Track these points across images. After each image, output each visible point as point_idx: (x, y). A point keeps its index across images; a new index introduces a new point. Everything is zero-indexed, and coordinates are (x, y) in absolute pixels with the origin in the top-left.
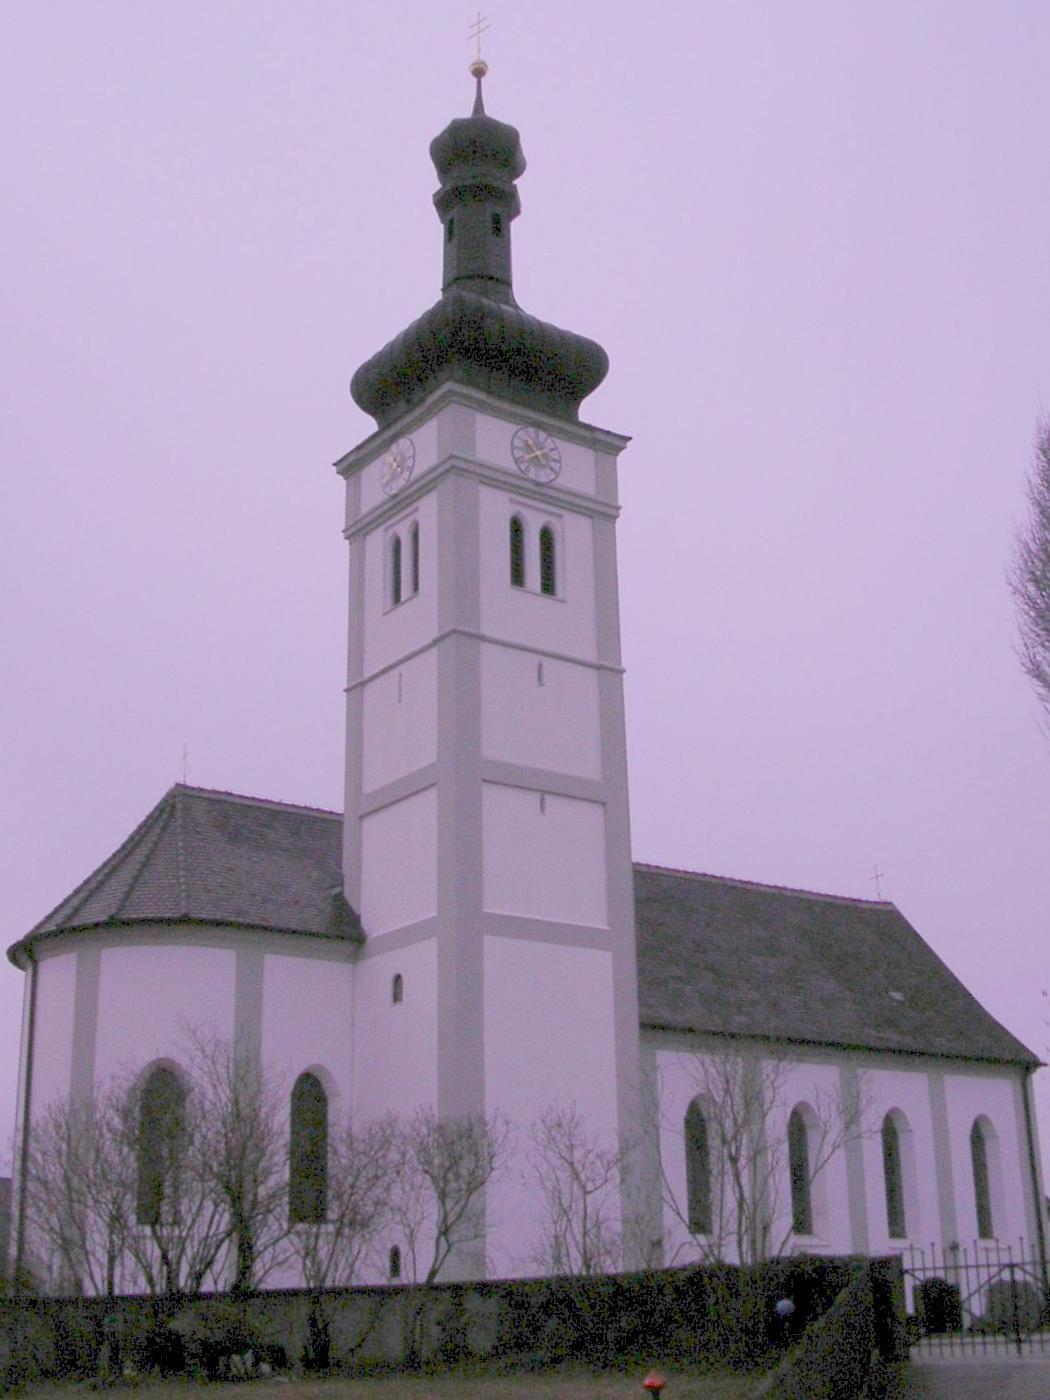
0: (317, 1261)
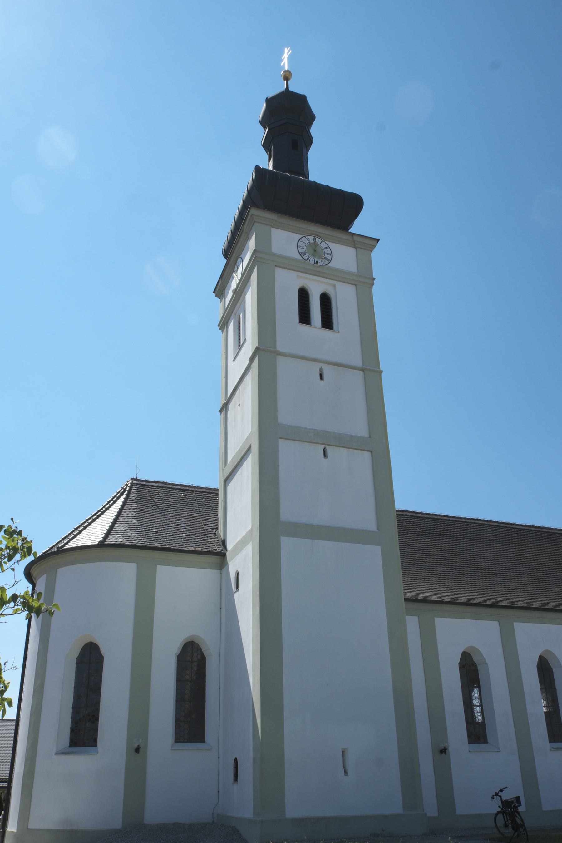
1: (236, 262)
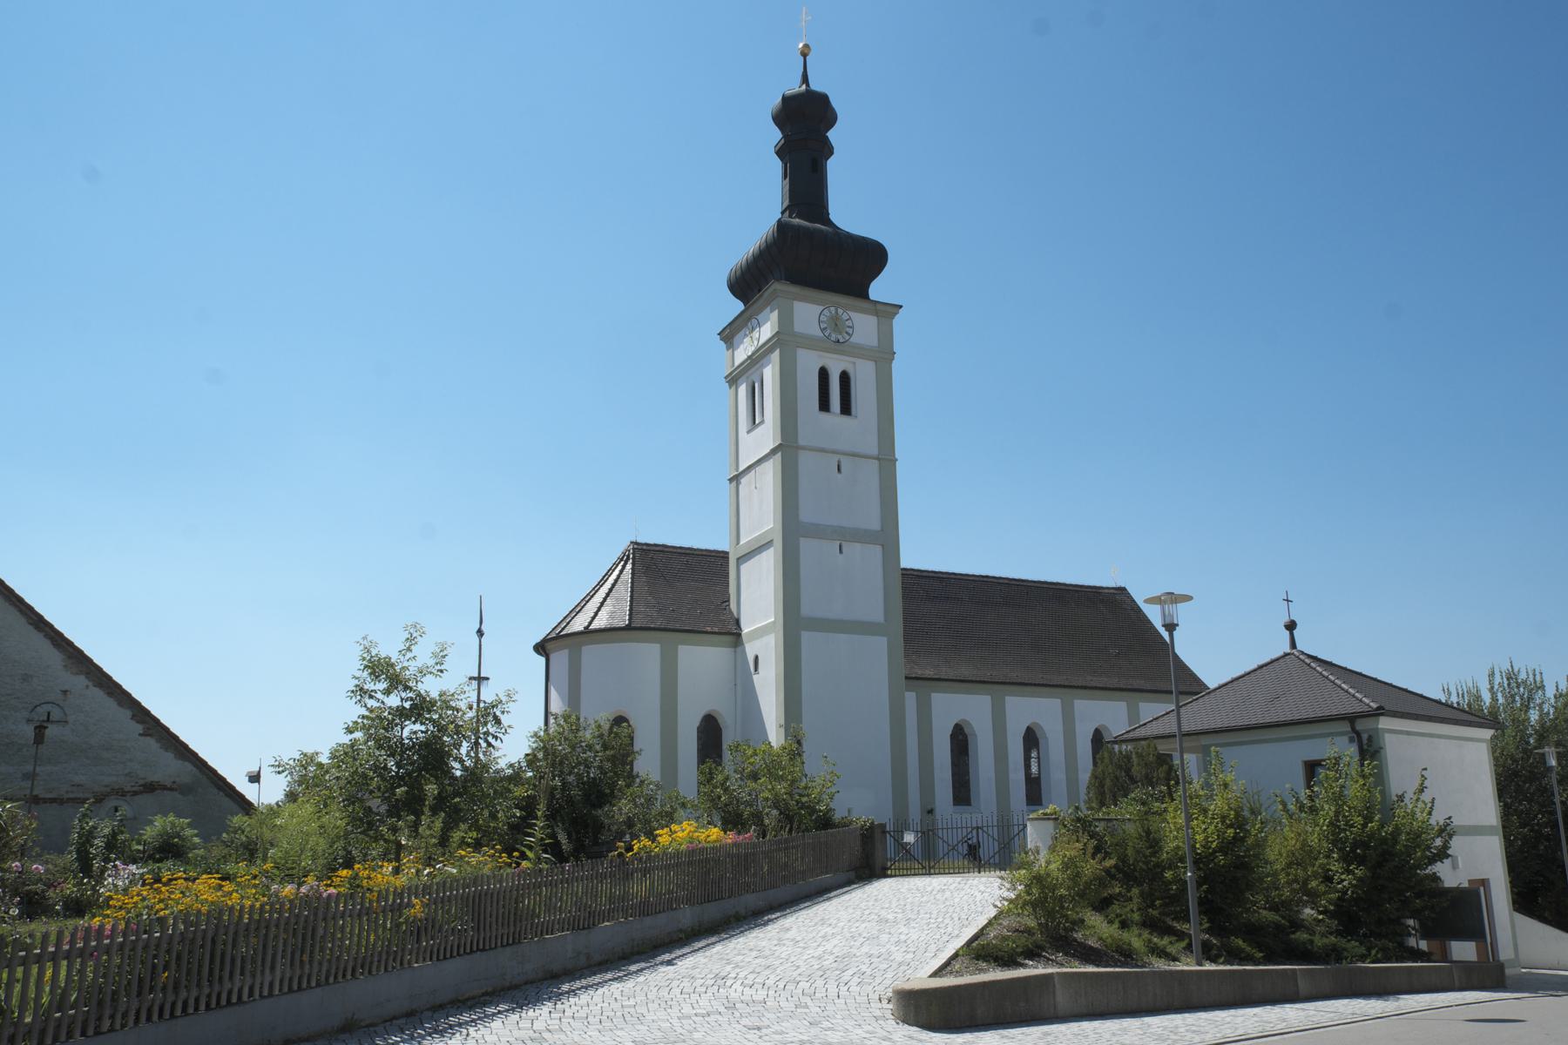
1: (749, 319)
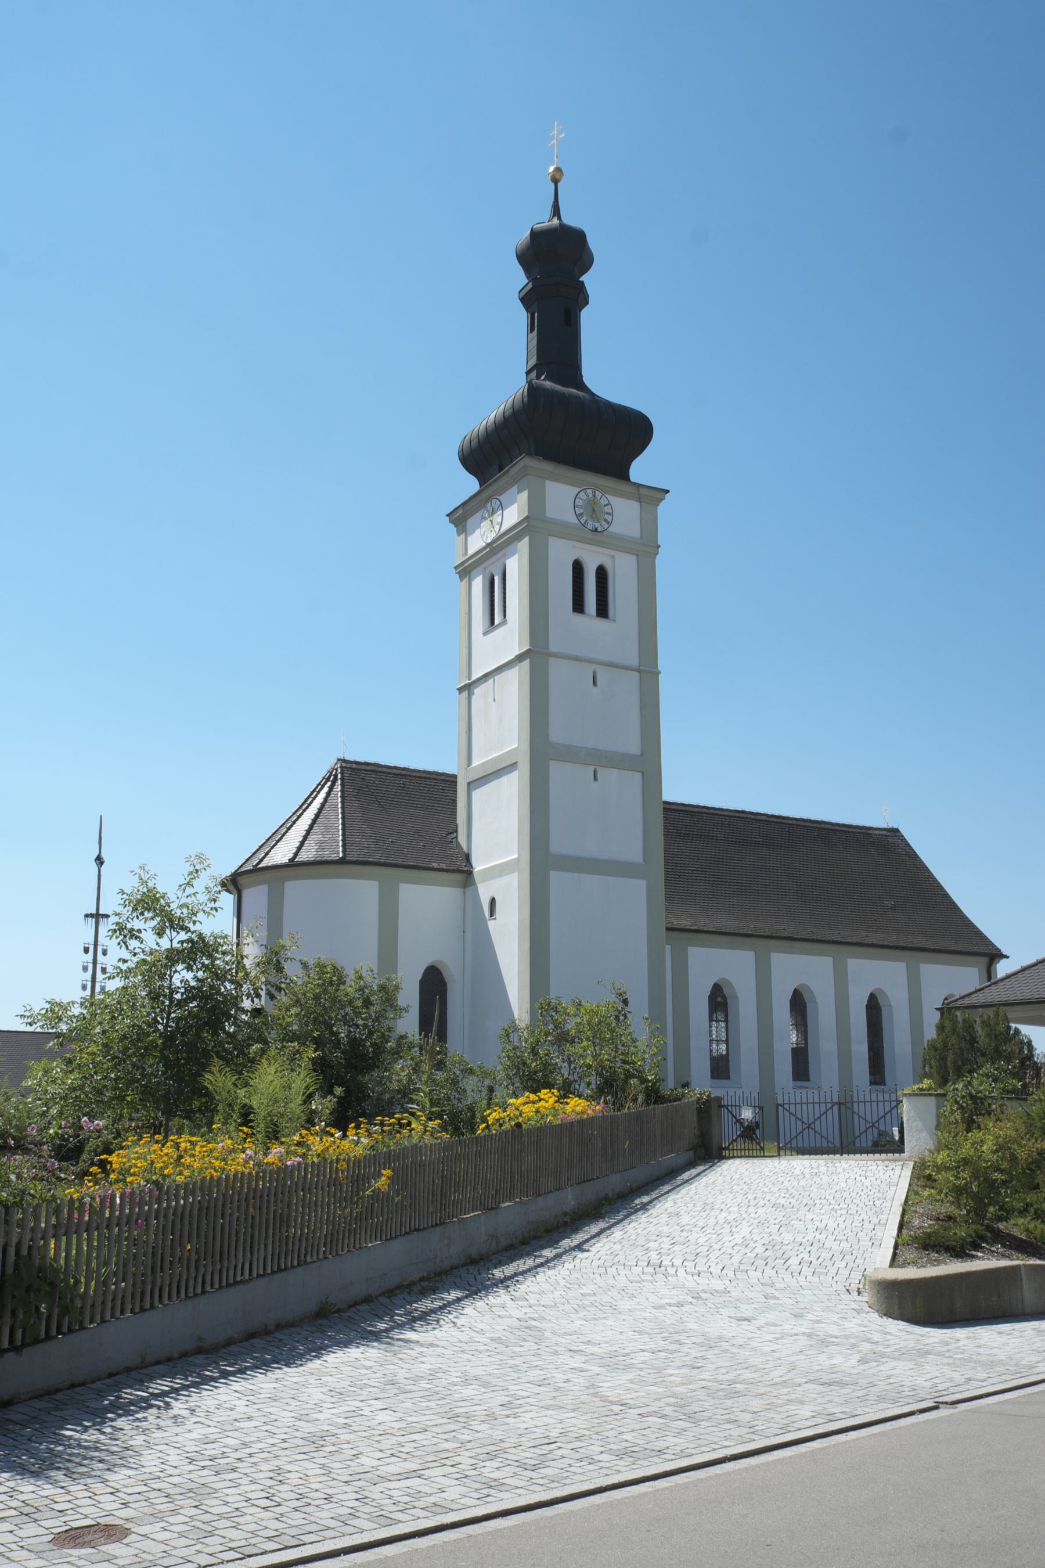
0: (941, 1406)
1: (489, 499)
